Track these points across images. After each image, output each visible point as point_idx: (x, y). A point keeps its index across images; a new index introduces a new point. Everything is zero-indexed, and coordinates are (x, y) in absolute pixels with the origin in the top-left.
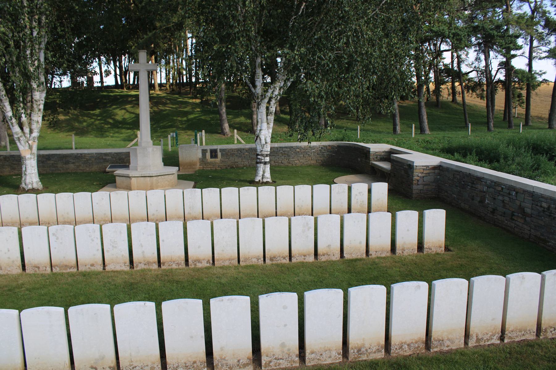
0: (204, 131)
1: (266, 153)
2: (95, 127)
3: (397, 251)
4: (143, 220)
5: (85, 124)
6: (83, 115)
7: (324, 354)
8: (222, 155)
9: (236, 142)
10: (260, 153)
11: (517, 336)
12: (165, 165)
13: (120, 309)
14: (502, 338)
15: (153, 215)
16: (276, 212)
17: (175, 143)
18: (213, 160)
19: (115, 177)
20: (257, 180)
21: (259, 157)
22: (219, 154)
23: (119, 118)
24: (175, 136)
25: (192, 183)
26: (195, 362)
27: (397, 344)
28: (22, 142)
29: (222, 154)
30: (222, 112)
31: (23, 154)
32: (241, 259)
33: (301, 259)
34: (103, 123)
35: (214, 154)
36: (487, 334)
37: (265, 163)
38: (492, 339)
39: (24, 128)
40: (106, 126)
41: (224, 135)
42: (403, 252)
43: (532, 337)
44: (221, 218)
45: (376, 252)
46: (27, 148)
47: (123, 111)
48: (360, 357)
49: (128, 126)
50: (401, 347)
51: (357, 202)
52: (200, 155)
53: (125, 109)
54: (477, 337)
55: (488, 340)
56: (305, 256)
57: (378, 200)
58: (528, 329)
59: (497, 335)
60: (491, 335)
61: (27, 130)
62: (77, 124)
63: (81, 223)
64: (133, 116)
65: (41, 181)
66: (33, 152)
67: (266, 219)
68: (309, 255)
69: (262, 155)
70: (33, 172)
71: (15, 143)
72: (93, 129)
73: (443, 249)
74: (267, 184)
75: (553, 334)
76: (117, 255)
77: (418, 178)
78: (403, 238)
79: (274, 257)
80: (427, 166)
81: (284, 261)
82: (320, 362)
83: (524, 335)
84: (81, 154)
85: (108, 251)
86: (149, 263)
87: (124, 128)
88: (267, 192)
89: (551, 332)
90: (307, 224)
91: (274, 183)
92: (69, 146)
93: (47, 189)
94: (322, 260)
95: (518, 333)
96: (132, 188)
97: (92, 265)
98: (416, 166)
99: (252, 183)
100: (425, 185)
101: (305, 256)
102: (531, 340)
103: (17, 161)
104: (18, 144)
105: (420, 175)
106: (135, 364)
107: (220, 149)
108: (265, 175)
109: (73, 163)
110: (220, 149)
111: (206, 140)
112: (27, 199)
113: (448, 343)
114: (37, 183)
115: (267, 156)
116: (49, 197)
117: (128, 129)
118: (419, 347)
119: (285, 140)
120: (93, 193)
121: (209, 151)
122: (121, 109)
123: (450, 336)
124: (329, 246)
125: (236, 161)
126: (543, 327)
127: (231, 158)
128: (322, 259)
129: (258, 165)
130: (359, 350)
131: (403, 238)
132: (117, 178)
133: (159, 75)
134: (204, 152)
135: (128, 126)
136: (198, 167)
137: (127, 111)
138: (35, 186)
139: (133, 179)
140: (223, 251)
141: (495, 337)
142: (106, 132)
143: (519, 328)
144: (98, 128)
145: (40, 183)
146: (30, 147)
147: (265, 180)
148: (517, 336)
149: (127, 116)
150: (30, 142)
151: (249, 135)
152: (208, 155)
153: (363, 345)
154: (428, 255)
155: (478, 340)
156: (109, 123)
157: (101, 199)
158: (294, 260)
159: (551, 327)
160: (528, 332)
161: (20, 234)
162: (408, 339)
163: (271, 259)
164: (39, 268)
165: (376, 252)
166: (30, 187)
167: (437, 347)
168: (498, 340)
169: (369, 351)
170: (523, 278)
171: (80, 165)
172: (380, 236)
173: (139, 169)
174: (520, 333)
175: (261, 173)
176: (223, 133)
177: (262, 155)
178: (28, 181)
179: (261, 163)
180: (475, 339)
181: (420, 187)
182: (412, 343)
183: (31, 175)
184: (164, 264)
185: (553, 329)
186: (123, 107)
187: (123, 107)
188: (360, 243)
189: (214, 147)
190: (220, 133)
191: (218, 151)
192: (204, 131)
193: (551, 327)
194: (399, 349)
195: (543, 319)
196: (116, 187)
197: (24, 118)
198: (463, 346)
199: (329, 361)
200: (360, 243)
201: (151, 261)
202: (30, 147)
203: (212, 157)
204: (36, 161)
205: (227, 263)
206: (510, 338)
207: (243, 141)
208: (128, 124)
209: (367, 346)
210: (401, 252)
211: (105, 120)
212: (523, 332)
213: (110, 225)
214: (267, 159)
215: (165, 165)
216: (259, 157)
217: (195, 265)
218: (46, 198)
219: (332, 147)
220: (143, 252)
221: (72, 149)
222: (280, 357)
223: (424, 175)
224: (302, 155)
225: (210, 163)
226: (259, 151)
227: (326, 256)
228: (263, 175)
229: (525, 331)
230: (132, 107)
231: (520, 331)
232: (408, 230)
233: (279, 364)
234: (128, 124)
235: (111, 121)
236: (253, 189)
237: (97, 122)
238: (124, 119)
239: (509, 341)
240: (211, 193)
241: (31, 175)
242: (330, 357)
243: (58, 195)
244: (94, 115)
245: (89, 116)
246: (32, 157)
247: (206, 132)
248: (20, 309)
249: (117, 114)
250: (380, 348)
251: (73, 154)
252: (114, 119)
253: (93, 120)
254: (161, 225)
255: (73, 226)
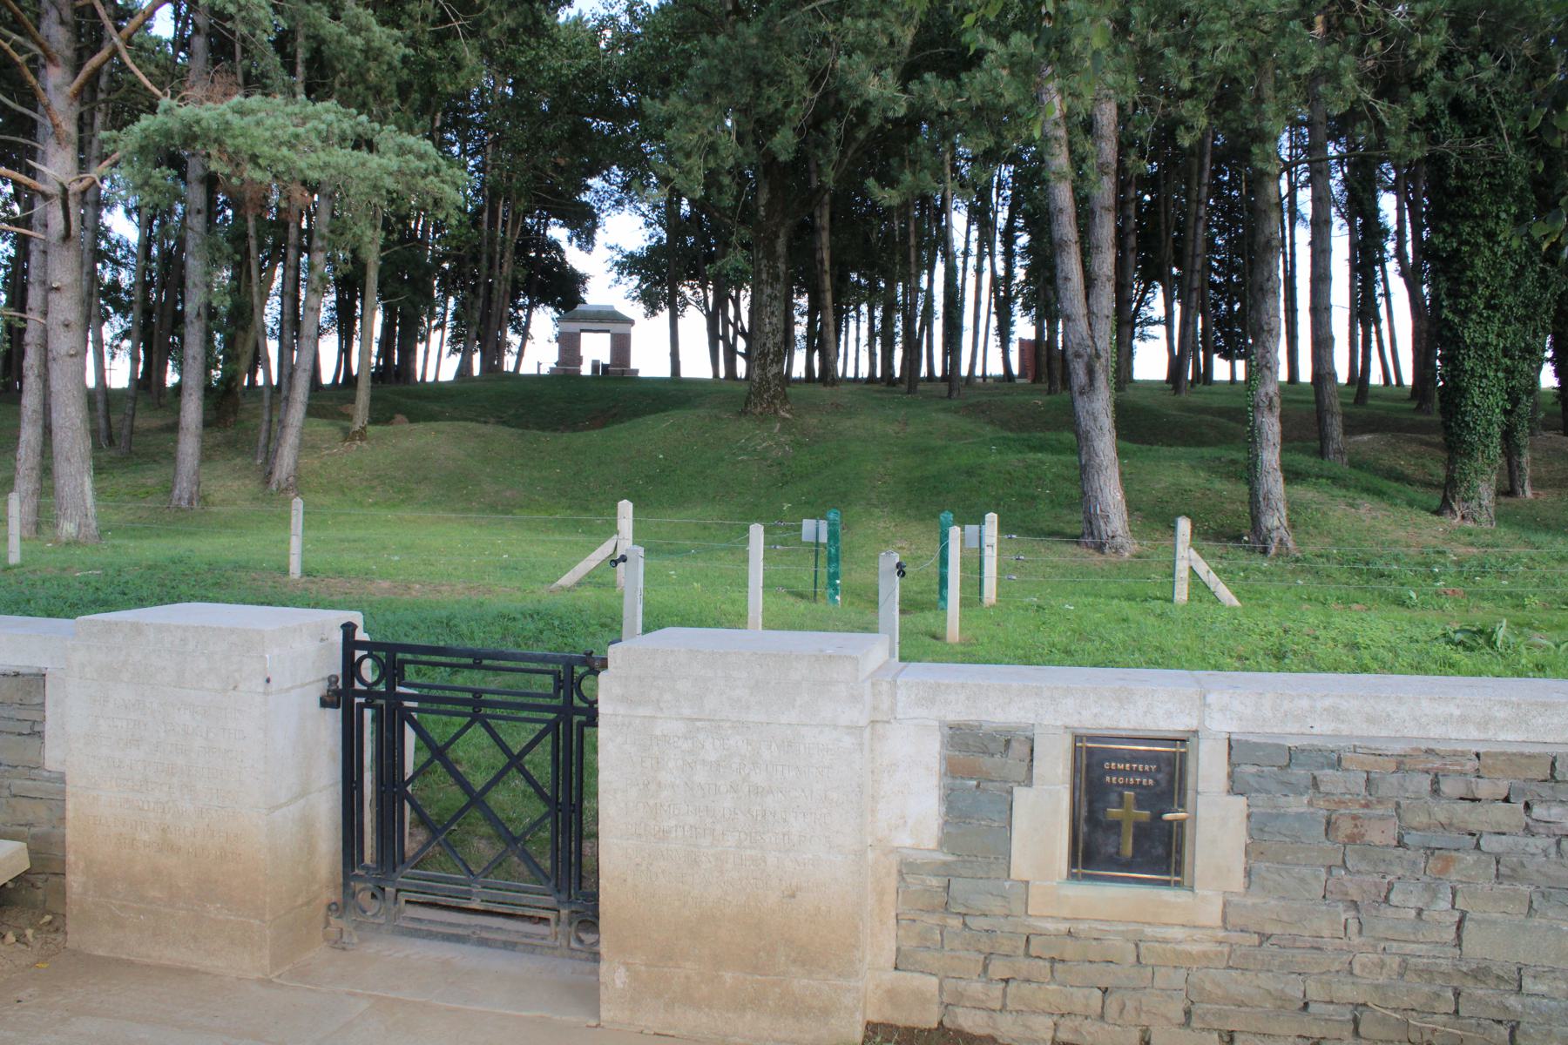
0: (992, 518)
8: (1263, 837)
9: (1182, 593)
17: (823, 578)
18: (1115, 901)
22: (1216, 822)
24: (824, 539)
29: (1258, 826)
35: (1126, 812)
41: (1100, 548)
52: (914, 812)
111: (1001, 570)
125: (1478, 945)
127: (1407, 899)
133: (852, 324)
134: (980, 767)
136: (877, 984)
152: (1043, 814)
176: (1088, 534)
190: (1075, 539)
191: (1208, 771)
192: (992, 518)
203: (1089, 855)
225: (1057, 956)
247: (1003, 527)
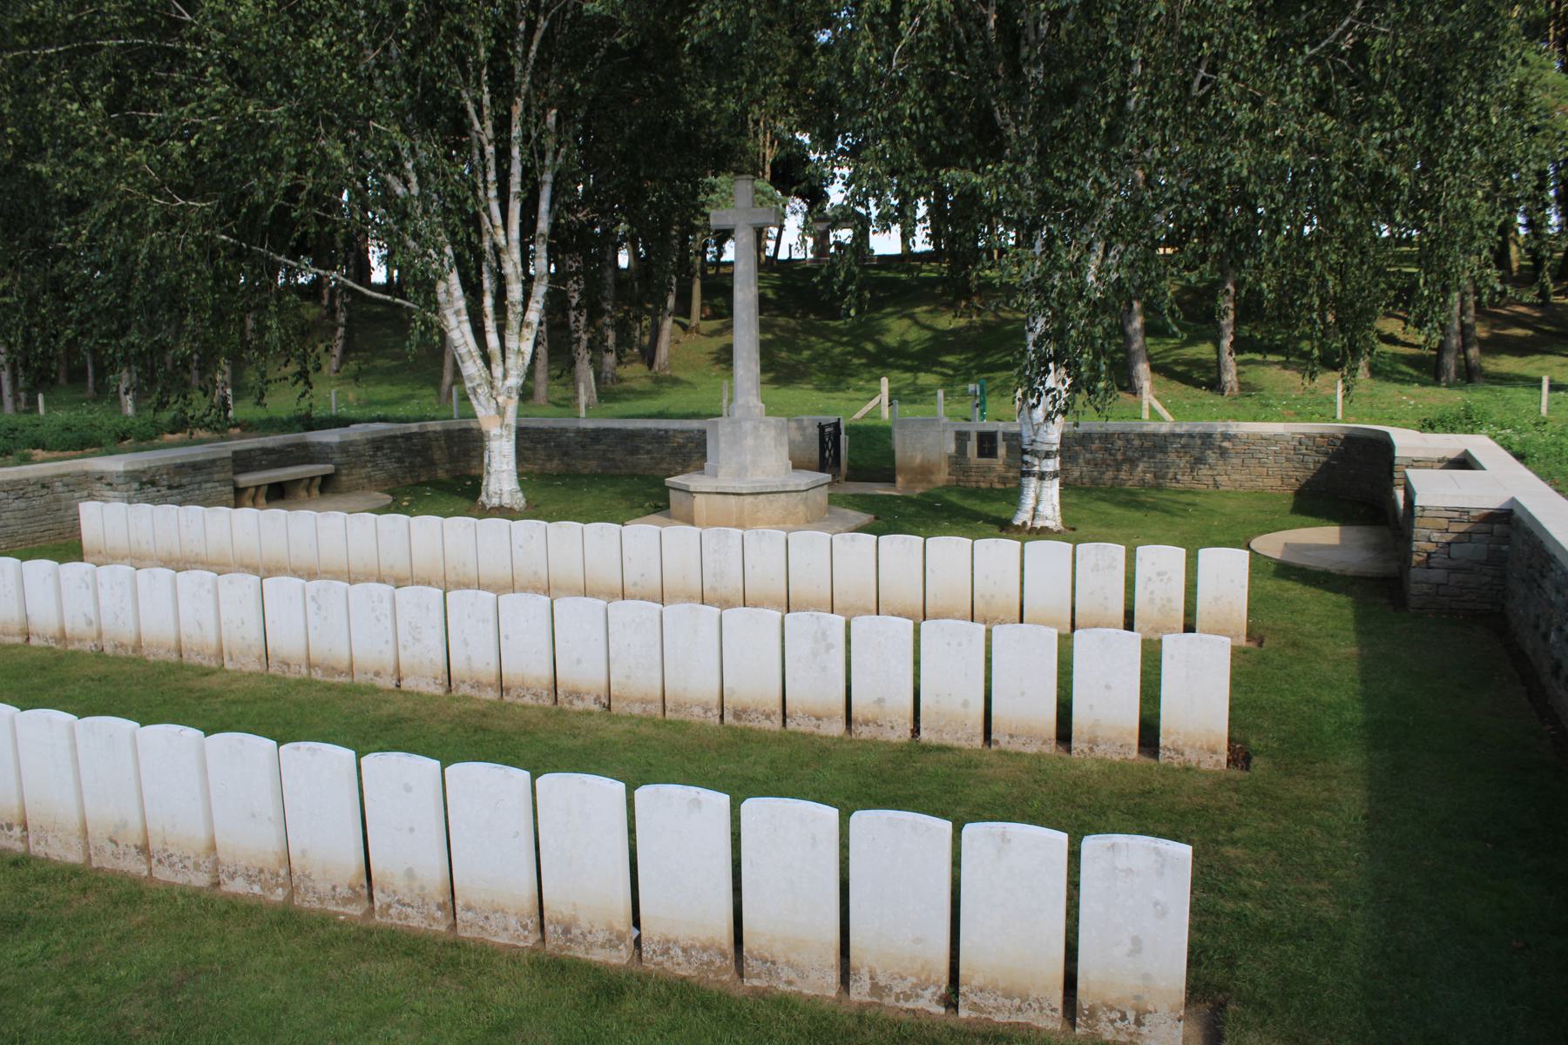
1: (1046, 448)
2: (827, 363)
3: (1074, 744)
4: (690, 599)
5: (806, 354)
6: (810, 330)
7: (492, 917)
10: (1029, 448)
11: (998, 1009)
12: (795, 467)
13: (374, 763)
14: (951, 999)
15: (635, 584)
16: (1073, 620)
18: (985, 460)
19: (666, 490)
20: (1017, 522)
21: (1027, 458)
23: (891, 340)
25: (865, 518)
26: (261, 871)
27: (656, 939)
28: (482, 398)
30: (1130, 330)
31: (485, 428)
32: (669, 705)
33: (807, 726)
34: (849, 353)
36: (903, 979)
37: (1042, 476)
38: (917, 996)
39: (493, 366)
40: (856, 361)
42: (1091, 749)
43: (929, 1003)
44: (1021, 621)
45: (1011, 736)
46: (493, 412)
47: (906, 322)
48: (569, 948)
49: (909, 363)
50: (666, 952)
51: (1152, 601)
52: (951, 448)
53: (911, 317)
54: (872, 978)
55: (907, 998)
56: (818, 719)
57: (1216, 599)
58: (1034, 995)
59: (932, 989)
60: (915, 986)
61: (498, 371)
62: (784, 354)
63: (803, 608)
64: (927, 334)
65: (522, 490)
66: (507, 421)
67: (996, 629)
68: (829, 717)
69: (1035, 453)
70: (505, 467)
71: (468, 399)
72: (822, 369)
73: (1224, 760)
74: (1043, 533)
75: (1118, 1031)
76: (1027, 707)
77: (1431, 547)
78: (1091, 707)
79: (744, 711)
80: (1465, 511)
81: (766, 725)
82: (485, 936)
83: (1019, 1009)
84: (666, 431)
85: (405, 647)
86: (478, 685)
87: (898, 367)
88: (1048, 557)
89: (1112, 1021)
90: (824, 634)
91: (1071, 532)
92: (714, 410)
93: (533, 511)
94: (863, 736)
95: (1001, 1000)
96: (697, 520)
97: (377, 674)
98: (1423, 509)
99: (1004, 527)
100: (1452, 570)
101: (818, 719)
102: (1039, 1030)
103: (469, 444)
104: (474, 402)
105: (1436, 536)
106: (171, 851)
107: (1004, 434)
108: (1040, 508)
109: (649, 452)
110: (1004, 434)
112: (495, 526)
113: (787, 973)
114: (511, 493)
115: (1048, 455)
116: (534, 527)
117: (907, 369)
118: (713, 963)
119: (1298, 414)
120: (977, 542)
121: (974, 437)
122: (904, 316)
123: (793, 957)
124: (880, 701)
126: (1084, 998)
128: (864, 732)
129: (1025, 480)
130: (567, 931)
131: (1091, 707)
132: (673, 494)
134: (961, 437)
135: (909, 363)
137: (917, 323)
138: (506, 501)
139: (698, 497)
140: (628, 677)
141: (928, 994)
142: (851, 376)
143: (1002, 985)
144: (835, 366)
145: (520, 495)
146: (501, 412)
147: (1039, 524)
148: (998, 1009)
149: (914, 335)
150: (500, 399)
151: (1203, 394)
152: (972, 447)
153: (575, 919)
154: (1168, 770)
155: (876, 988)
156: (865, 353)
157: (641, 541)
158: (791, 725)
159: (1111, 1009)
160: (1035, 1005)
161: (917, 632)
162: (683, 934)
163: (737, 715)
164: (288, 665)
165: (1011, 736)
166: (495, 501)
167: (758, 976)
168: (938, 1002)
169: (589, 937)
170: (1004, 838)
171: (663, 459)
172: (1023, 694)
173: (721, 473)
174: (1008, 1002)
175: (1029, 501)
177: (1035, 453)
178: (492, 488)
179: (1029, 474)
180: (866, 984)
181: (1437, 575)
182: (693, 946)
183: (501, 473)
184: (508, 690)
185: (1115, 1015)
186: (908, 311)
187: (908, 311)
188: (965, 704)
189: (988, 426)
191: (1000, 437)
193: (1111, 1009)
194: (662, 954)
195: (1080, 975)
196: (669, 516)
197: (492, 340)
198: (833, 993)
199: (503, 939)
200: (965, 704)
201: (484, 681)
202: (501, 412)
203: (981, 454)
204: (513, 443)
205: (637, 710)
206: (975, 1007)
207: (1165, 414)
208: (911, 356)
209: (584, 924)
210: (1085, 747)
211: (856, 346)
212: (1017, 1002)
213: (621, 602)
214: (1052, 465)
215: (795, 467)
216: (1027, 458)
217: (571, 703)
218: (530, 530)
219: (1330, 439)
220: (469, 658)
221: (451, 418)
222: (407, 901)
223: (1449, 537)
224: (1239, 461)
226: (1026, 440)
227: (872, 727)
228: (1035, 509)
229: (1024, 998)
230: (930, 312)
231: (1008, 995)
232: (1108, 687)
233: (407, 917)
234: (911, 356)
235: (870, 347)
236: (1009, 546)
237: (838, 350)
238: (905, 343)
239: (974, 1015)
240: (901, 548)
241: (501, 473)
242: (506, 929)
243: (980, 544)
244: (836, 331)
245: (823, 333)
246: (505, 433)
248: (280, 742)
249: (889, 330)
250: (613, 937)
251: (648, 430)
252: (877, 343)
253: (829, 344)
254: (860, 624)
255: (779, 614)
